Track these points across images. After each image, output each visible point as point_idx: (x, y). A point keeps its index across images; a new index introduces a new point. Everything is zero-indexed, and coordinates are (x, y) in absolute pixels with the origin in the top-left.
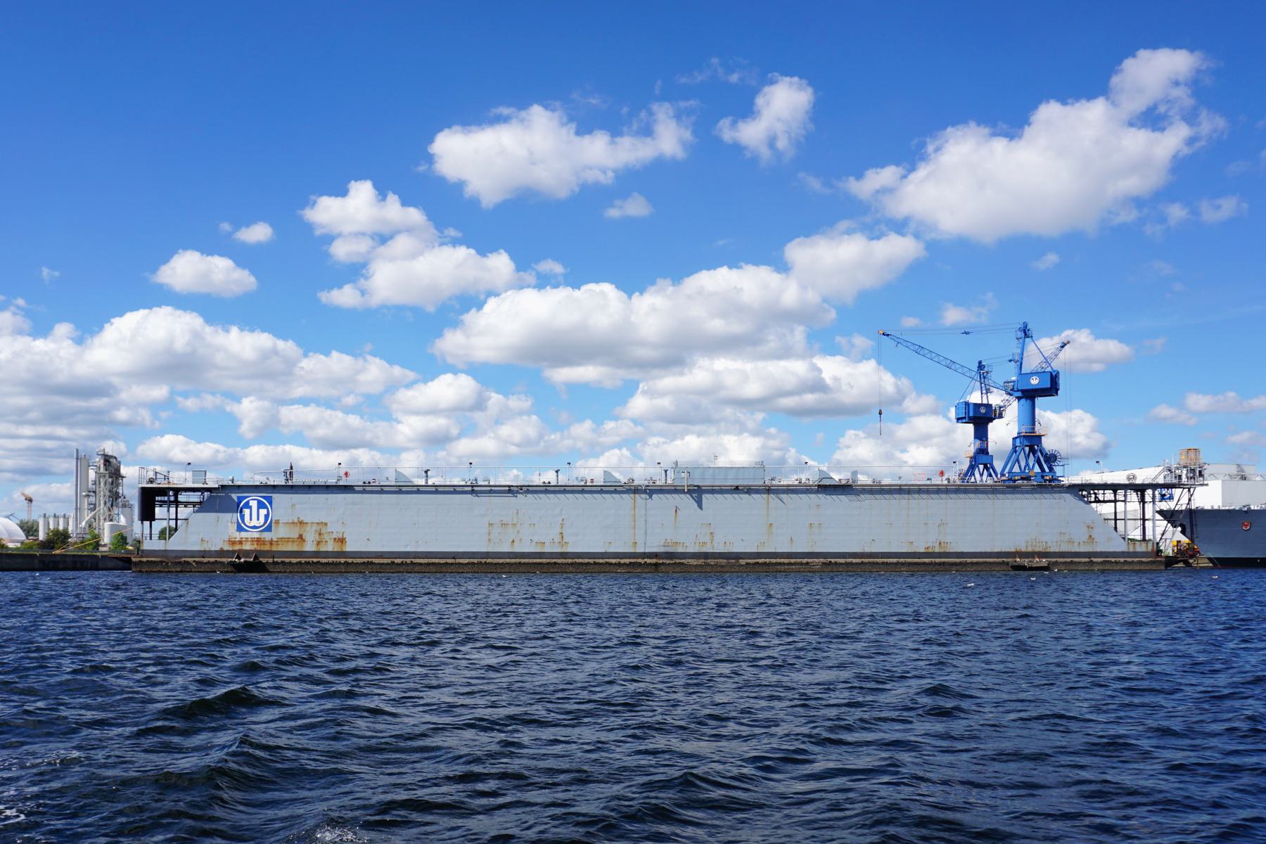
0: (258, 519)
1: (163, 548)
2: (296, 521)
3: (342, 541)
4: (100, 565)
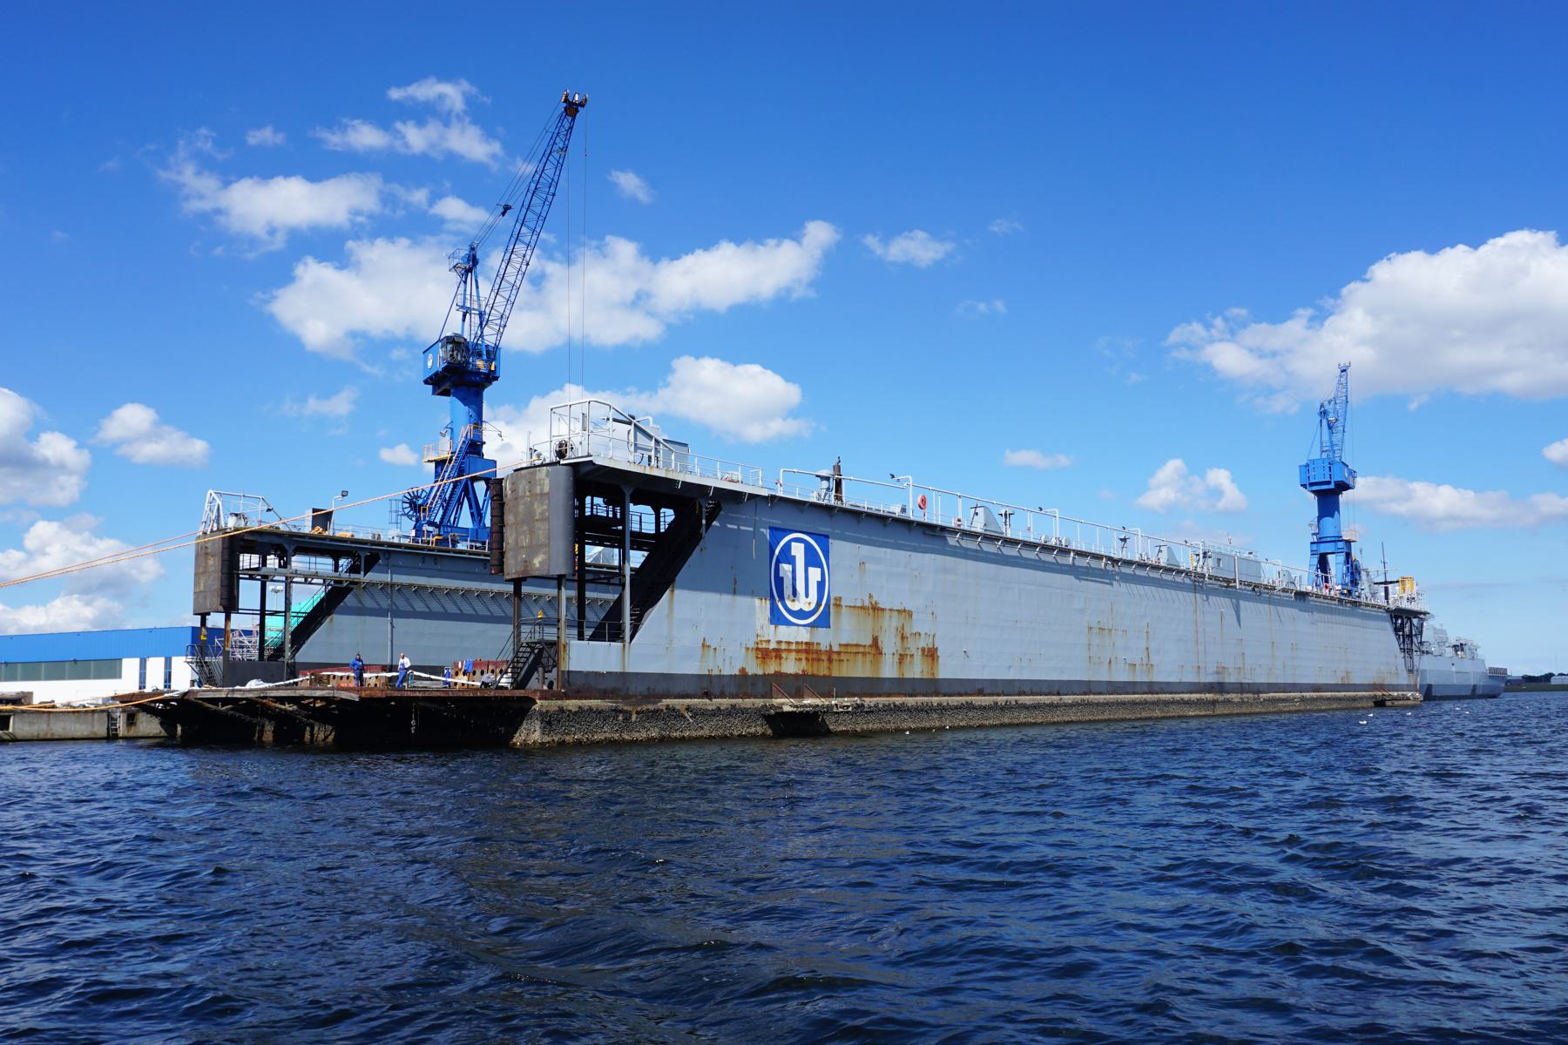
0: (807, 595)
1: (615, 667)
2: (867, 603)
3: (931, 654)
4: (986, 691)
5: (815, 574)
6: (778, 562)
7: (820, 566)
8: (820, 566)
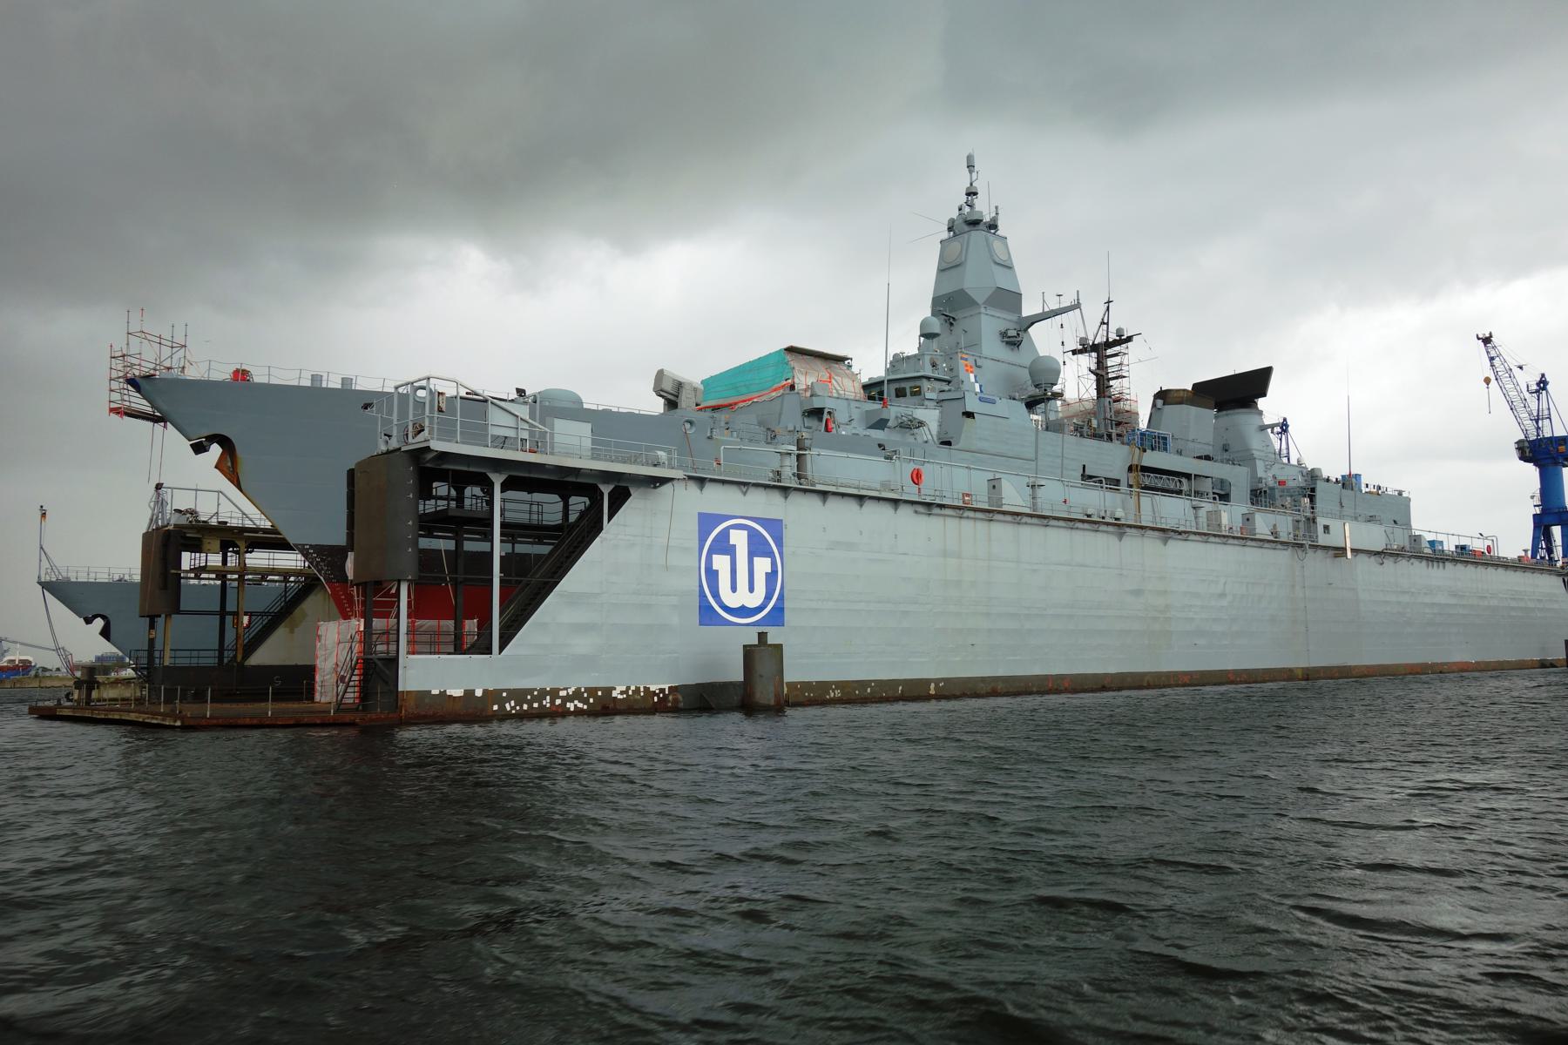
0: (751, 589)
5: (763, 565)
6: (711, 552)
7: (770, 554)
8: (770, 554)
